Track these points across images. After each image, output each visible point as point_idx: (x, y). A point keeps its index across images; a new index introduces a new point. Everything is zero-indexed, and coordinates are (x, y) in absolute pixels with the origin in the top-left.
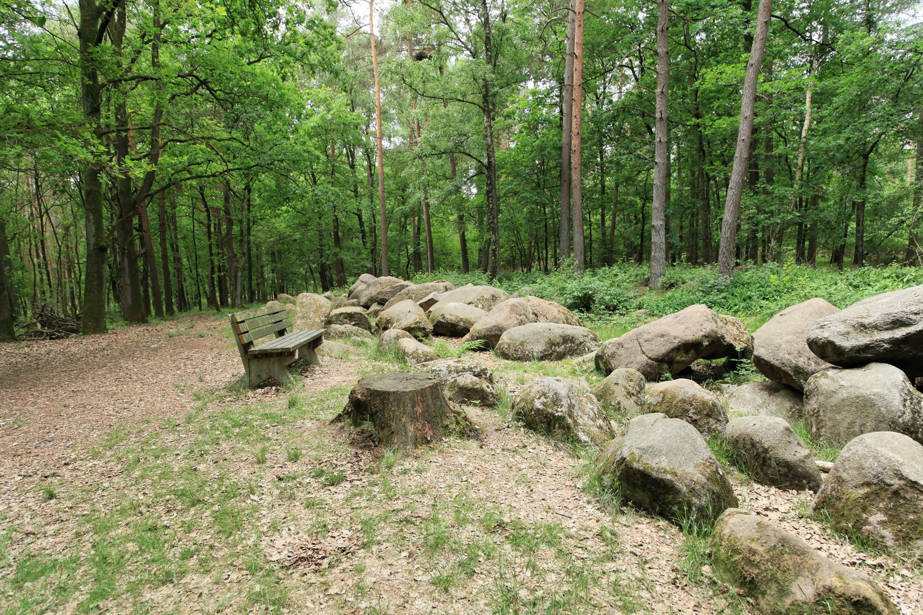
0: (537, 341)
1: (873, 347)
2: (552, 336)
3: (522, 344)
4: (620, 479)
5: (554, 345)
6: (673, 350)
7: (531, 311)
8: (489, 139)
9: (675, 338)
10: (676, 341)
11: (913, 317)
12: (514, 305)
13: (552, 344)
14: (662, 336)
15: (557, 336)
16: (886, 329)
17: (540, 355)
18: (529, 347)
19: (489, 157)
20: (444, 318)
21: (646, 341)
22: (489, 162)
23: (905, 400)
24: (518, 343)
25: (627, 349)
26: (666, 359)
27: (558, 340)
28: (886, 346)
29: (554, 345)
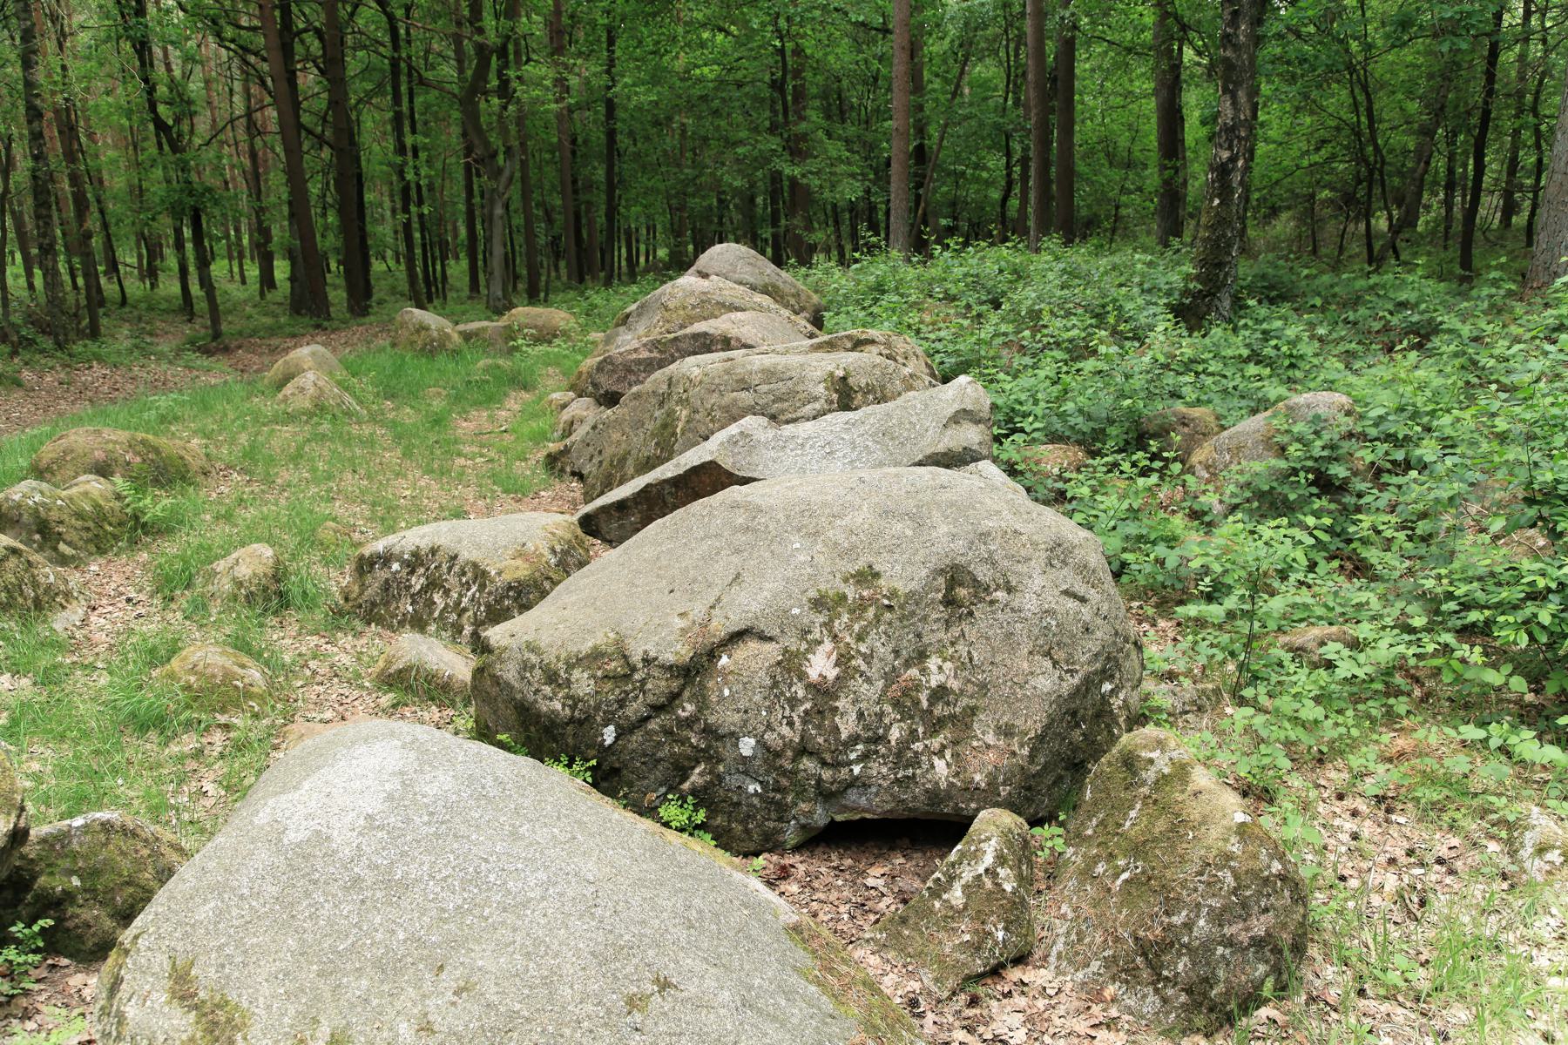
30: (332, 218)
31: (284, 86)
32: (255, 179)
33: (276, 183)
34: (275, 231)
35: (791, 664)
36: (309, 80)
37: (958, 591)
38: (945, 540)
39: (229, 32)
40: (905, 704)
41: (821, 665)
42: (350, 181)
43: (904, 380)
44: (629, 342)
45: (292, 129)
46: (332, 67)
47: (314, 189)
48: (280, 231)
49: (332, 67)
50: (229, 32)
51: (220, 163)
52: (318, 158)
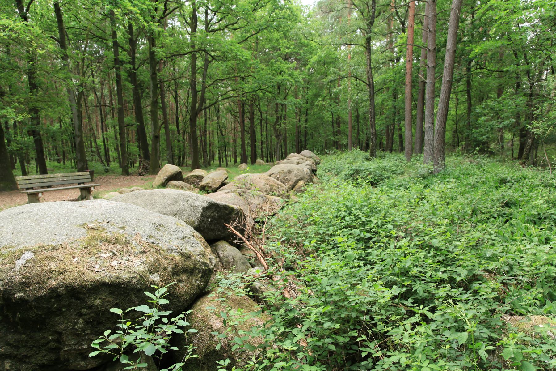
19: (369, 79)
22: (369, 82)
30: (249, 148)
31: (242, 124)
32: (235, 141)
33: (239, 141)
34: (238, 151)
35: (276, 176)
36: (247, 122)
37: (289, 172)
38: (289, 168)
39: (233, 113)
40: (284, 179)
41: (278, 176)
42: (253, 140)
43: (46, 115)
44: (115, 112)
45: (243, 131)
46: (251, 119)
47: (246, 142)
48: (239, 151)
49: (251, 119)
50: (233, 113)
51: (230, 137)
52: (247, 136)
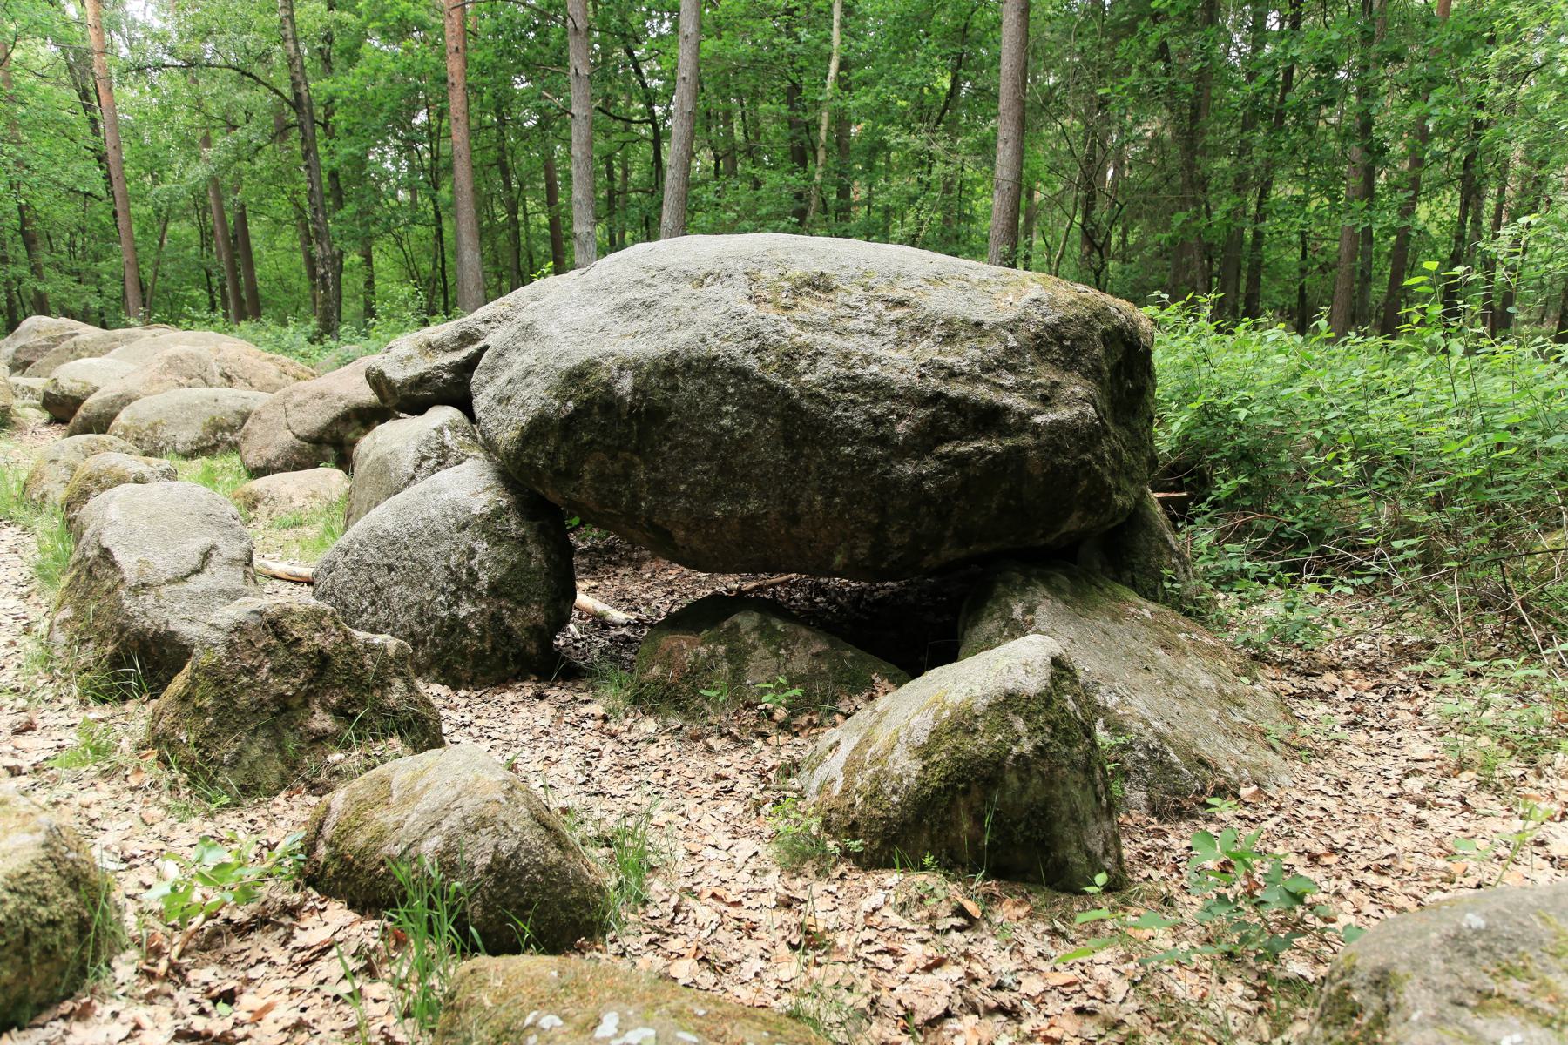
0: (187, 421)
1: (430, 380)
2: (217, 414)
3: (153, 428)
4: (915, 803)
5: (223, 429)
6: (335, 420)
7: (217, 371)
8: (291, 46)
9: (340, 399)
10: (341, 405)
11: (482, 327)
12: (177, 357)
13: (217, 427)
14: (323, 396)
15: (229, 411)
16: (454, 349)
17: (190, 447)
18: (168, 433)
19: (295, 85)
20: (56, 386)
21: (296, 406)
22: (298, 95)
23: (424, 458)
24: (145, 426)
25: (265, 421)
26: (327, 437)
27: (231, 420)
28: (446, 376)
29: (223, 429)
